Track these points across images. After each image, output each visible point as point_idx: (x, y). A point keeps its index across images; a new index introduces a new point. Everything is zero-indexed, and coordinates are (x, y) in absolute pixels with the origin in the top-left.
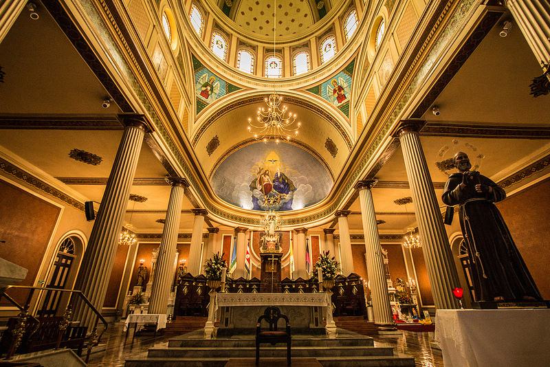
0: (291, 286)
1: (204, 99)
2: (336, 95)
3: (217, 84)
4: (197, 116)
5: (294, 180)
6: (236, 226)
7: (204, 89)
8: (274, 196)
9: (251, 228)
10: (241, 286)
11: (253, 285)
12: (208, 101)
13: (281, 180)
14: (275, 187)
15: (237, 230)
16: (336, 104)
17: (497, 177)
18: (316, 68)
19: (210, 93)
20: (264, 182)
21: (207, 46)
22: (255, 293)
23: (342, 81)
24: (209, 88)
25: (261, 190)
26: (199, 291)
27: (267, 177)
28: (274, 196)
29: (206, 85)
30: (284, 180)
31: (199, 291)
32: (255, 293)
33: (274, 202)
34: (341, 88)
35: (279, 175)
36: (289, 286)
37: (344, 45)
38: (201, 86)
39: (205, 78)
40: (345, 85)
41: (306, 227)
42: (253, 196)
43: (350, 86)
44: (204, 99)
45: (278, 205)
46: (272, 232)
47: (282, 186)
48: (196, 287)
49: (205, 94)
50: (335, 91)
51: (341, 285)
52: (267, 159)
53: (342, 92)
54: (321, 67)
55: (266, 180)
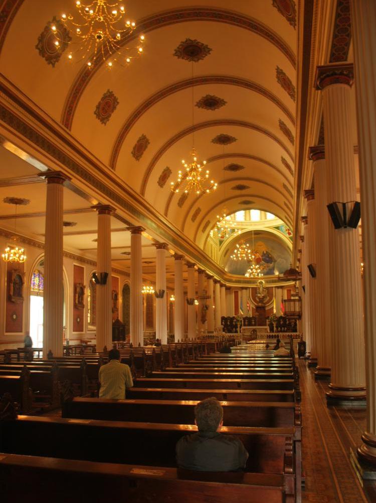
2: (287, 232)
13: (266, 255)
14: (263, 260)
16: (287, 235)
35: (265, 252)
47: (267, 259)
50: (286, 230)
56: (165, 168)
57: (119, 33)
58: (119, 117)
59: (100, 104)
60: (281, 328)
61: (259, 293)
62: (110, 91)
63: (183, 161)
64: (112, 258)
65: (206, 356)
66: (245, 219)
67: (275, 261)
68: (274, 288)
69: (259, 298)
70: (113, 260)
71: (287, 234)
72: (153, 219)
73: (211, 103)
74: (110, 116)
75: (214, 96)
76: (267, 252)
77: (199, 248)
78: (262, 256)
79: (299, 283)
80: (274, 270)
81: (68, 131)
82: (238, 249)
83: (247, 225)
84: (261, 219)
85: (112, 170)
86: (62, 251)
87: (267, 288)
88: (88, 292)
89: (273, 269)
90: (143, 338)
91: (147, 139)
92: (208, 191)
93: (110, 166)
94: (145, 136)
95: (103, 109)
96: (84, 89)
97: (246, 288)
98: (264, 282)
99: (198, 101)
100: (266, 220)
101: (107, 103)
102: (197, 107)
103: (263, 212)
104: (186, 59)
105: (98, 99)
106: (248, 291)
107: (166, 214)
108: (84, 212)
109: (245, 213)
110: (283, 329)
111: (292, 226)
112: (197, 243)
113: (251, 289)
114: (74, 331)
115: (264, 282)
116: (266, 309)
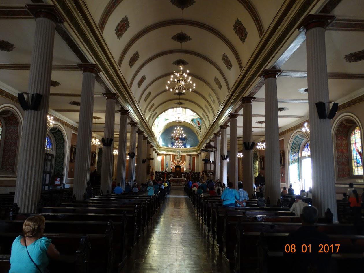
2: (198, 123)
34: (199, 122)
40: (200, 121)
41: (191, 154)
50: (197, 122)
56: (143, 75)
58: (128, 36)
59: (119, 24)
61: (177, 158)
62: (127, 17)
64: (253, 134)
69: (177, 161)
70: (253, 135)
71: (198, 125)
72: (132, 106)
73: (181, 38)
74: (123, 34)
75: (185, 34)
77: (149, 126)
81: (101, 33)
82: (175, 130)
85: (118, 66)
86: (106, 113)
87: (182, 155)
90: (75, 161)
91: (138, 55)
92: (171, 90)
93: (118, 64)
94: (138, 52)
95: (120, 28)
96: (113, 11)
97: (169, 155)
98: (180, 152)
99: (174, 35)
101: (123, 25)
102: (172, 39)
103: (184, 109)
104: (176, 6)
105: (118, 21)
106: (170, 155)
107: (139, 102)
108: (316, 4)
109: (279, 102)
112: (149, 123)
113: (171, 155)
114: (68, 178)
115: (180, 152)
116: (181, 167)
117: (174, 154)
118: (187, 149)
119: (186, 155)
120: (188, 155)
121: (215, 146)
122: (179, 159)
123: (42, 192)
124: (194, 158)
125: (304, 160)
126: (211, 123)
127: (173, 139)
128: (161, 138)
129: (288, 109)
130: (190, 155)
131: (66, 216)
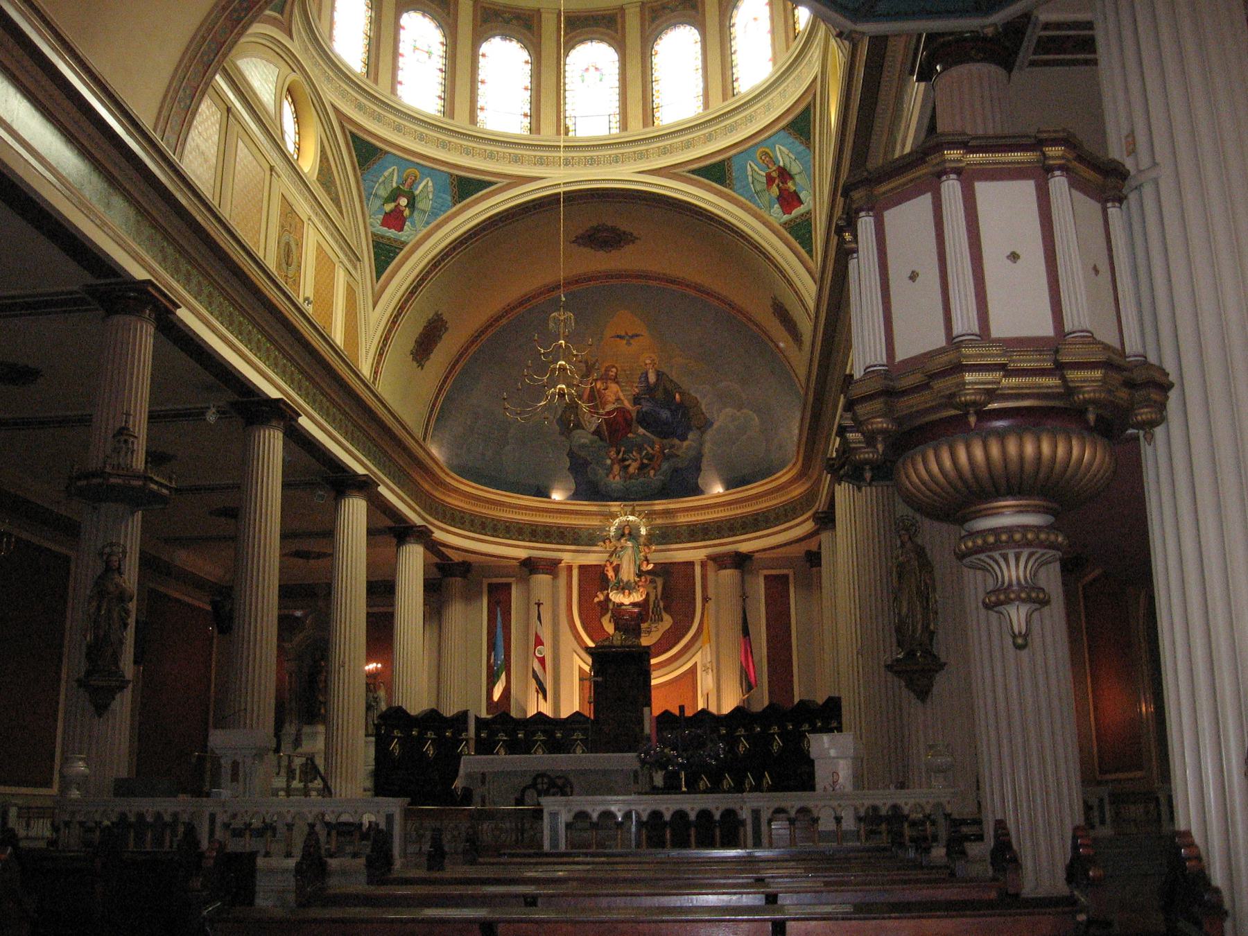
0: (512, 733)
1: (391, 233)
2: (775, 191)
3: (425, 187)
4: (377, 287)
5: (703, 395)
6: (523, 554)
7: (389, 207)
8: (640, 449)
9: (570, 557)
10: (540, 737)
11: (534, 734)
12: (403, 236)
13: (660, 395)
14: (644, 420)
15: (530, 566)
16: (777, 214)
17: (536, 712)
18: (718, 106)
19: (407, 212)
20: (604, 404)
21: (387, 92)
22: (579, 750)
23: (784, 154)
24: (403, 202)
25: (597, 432)
26: (429, 749)
27: (614, 387)
28: (640, 449)
29: (394, 196)
30: (669, 394)
31: (429, 749)
32: (579, 750)
33: (642, 467)
34: (784, 174)
35: (652, 378)
36: (544, 732)
37: (788, 48)
38: (378, 203)
39: (391, 176)
40: (795, 168)
41: (745, 548)
42: (571, 454)
43: (808, 171)
44: (391, 233)
45: (654, 477)
46: (628, 573)
47: (665, 414)
48: (421, 741)
49: (395, 219)
50: (770, 180)
51: (741, 731)
52: (608, 333)
53: (790, 184)
54: (731, 104)
55: (612, 398)
57: (306, 616)
60: (985, 541)
63: (379, 665)
65: (619, 850)
66: (535, 128)
67: (705, 425)
68: (562, 847)
76: (659, 375)
78: (636, 400)
79: (851, 432)
80: (699, 469)
83: (541, 162)
84: (624, 125)
88: (1107, 807)
89: (696, 466)
100: (650, 132)
110: (980, 542)
111: (846, 49)
117: (593, 558)
118: (708, 507)
119: (703, 564)
120: (719, 561)
121: (1105, 211)
122: (637, 597)
123: (444, 518)
124: (777, 587)
125: (656, 48)
126: (239, 140)
127: (578, 426)
128: (1073, 191)
129: (776, 299)
130: (741, 561)
131: (427, 636)
